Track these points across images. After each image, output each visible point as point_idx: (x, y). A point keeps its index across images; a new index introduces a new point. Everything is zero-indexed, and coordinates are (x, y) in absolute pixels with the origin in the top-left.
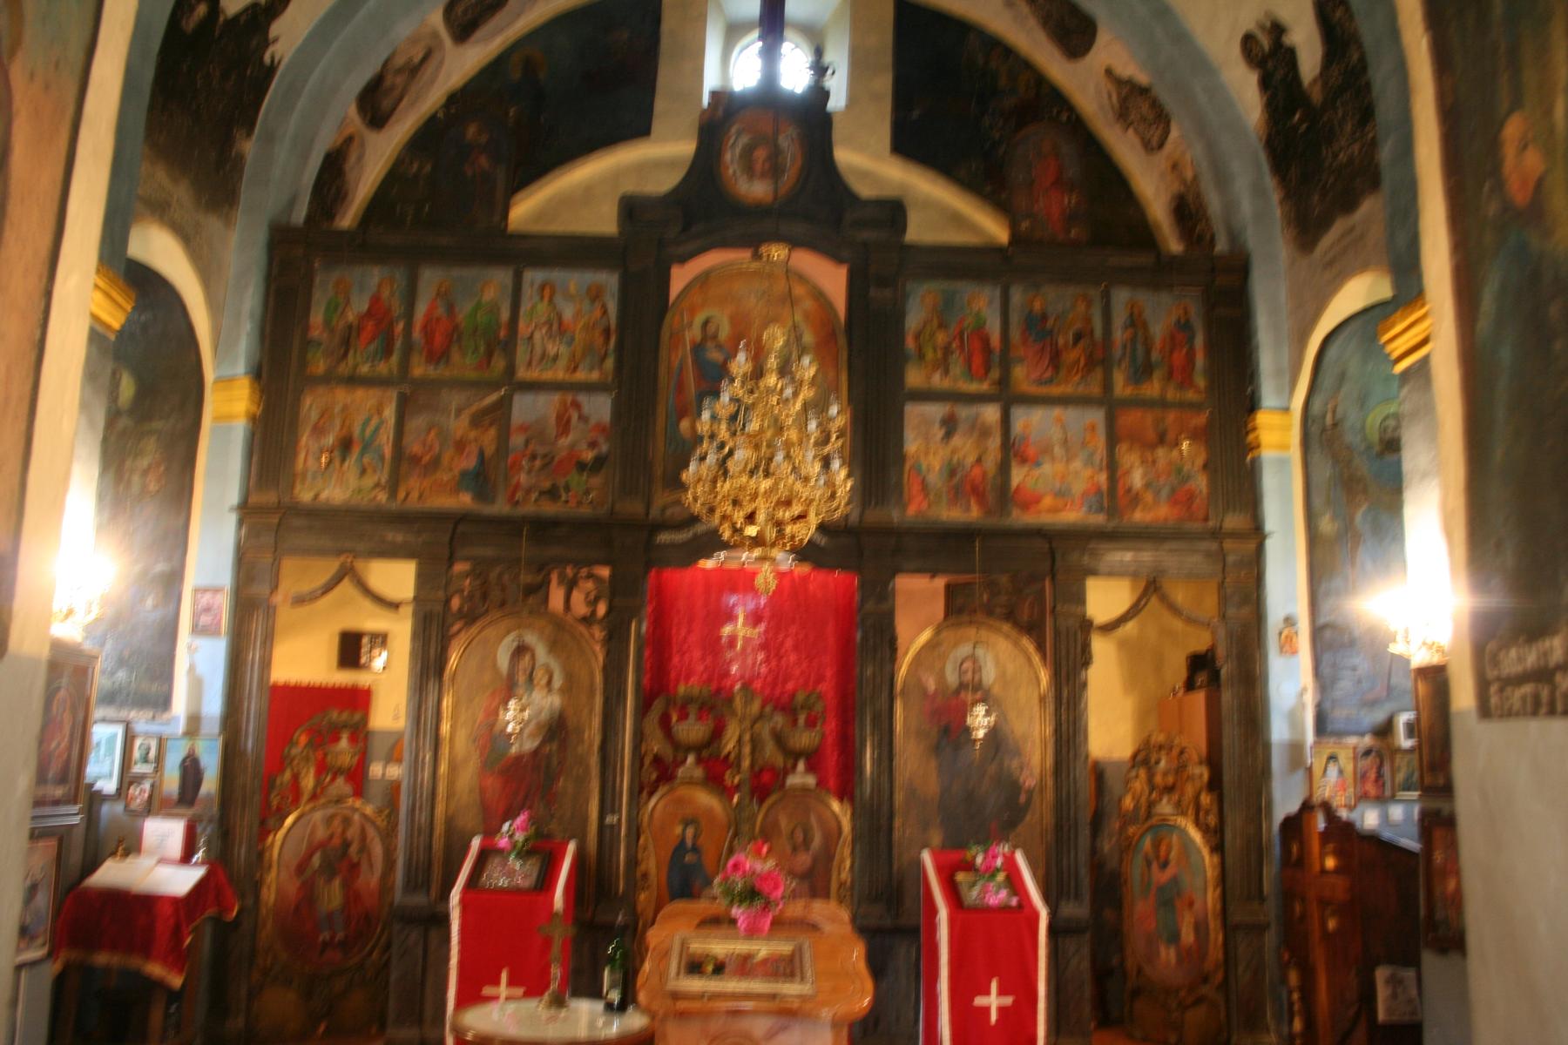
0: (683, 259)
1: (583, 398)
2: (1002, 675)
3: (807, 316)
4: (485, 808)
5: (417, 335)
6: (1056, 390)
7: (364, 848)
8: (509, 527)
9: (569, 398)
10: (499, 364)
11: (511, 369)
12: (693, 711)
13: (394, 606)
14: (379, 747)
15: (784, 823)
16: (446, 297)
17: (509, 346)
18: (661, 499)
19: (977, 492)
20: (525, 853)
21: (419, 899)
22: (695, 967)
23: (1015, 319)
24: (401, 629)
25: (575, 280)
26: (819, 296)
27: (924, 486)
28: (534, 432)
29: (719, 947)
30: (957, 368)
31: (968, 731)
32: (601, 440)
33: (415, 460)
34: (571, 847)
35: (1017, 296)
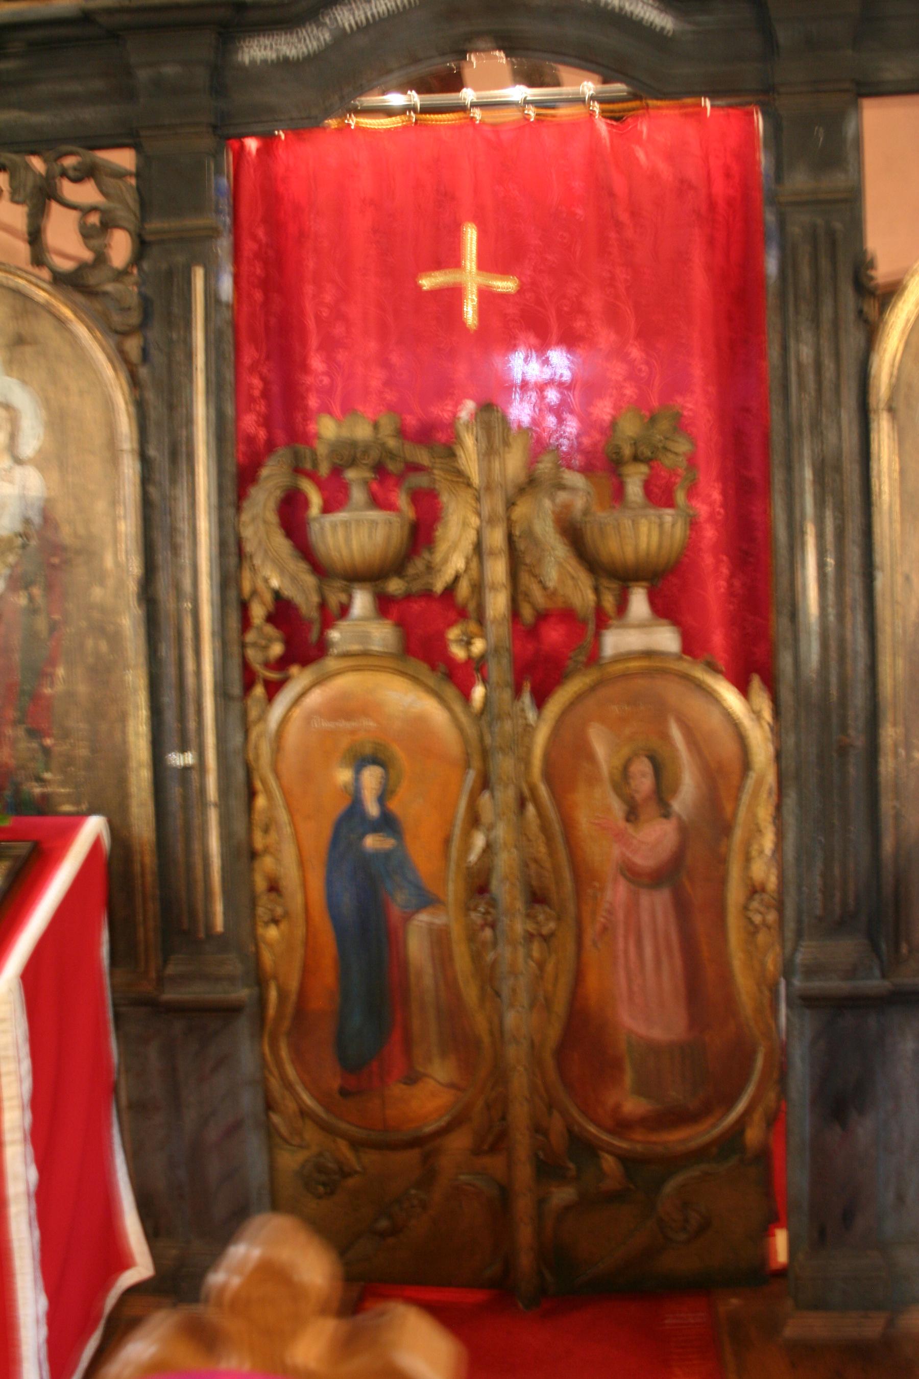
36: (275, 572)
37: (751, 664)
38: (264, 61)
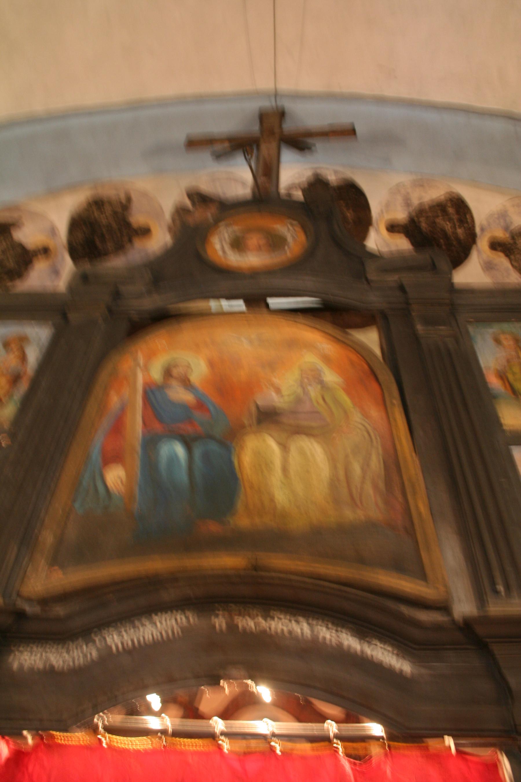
38: (32, 670)
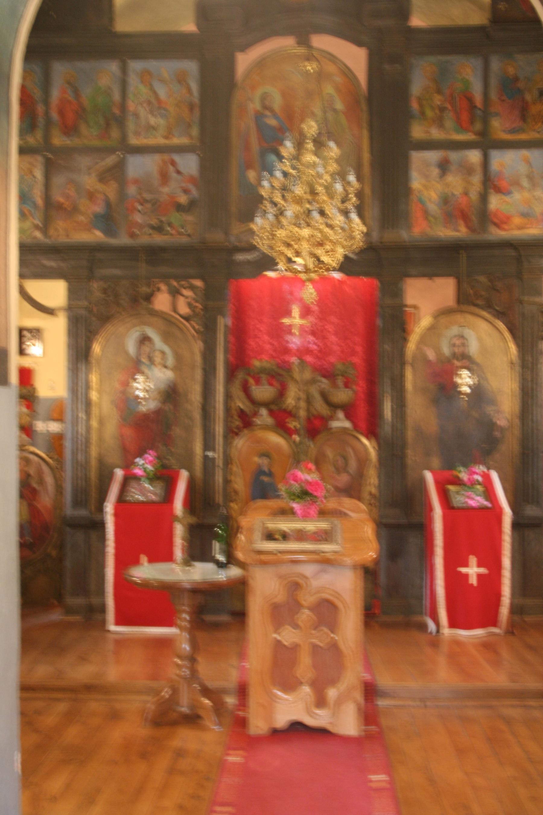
0: (244, 48)
1: (177, 158)
2: (484, 350)
3: (338, 90)
4: (125, 449)
5: (55, 116)
6: (523, 137)
7: (41, 481)
8: (129, 254)
9: (166, 157)
10: (115, 133)
11: (124, 137)
12: (264, 377)
13: (49, 311)
14: (41, 409)
15: (330, 453)
16: (72, 85)
17: (121, 122)
18: (237, 229)
19: (465, 217)
20: (153, 478)
21: (82, 512)
22: (270, 536)
23: (494, 82)
24: (57, 329)
25: (166, 68)
26: (347, 73)
27: (426, 213)
28: (143, 184)
29: (285, 525)
30: (449, 123)
31: (455, 386)
32: (191, 187)
33: (60, 207)
34: (184, 475)
35: (495, 64)
36: (241, 403)
37: (372, 432)
